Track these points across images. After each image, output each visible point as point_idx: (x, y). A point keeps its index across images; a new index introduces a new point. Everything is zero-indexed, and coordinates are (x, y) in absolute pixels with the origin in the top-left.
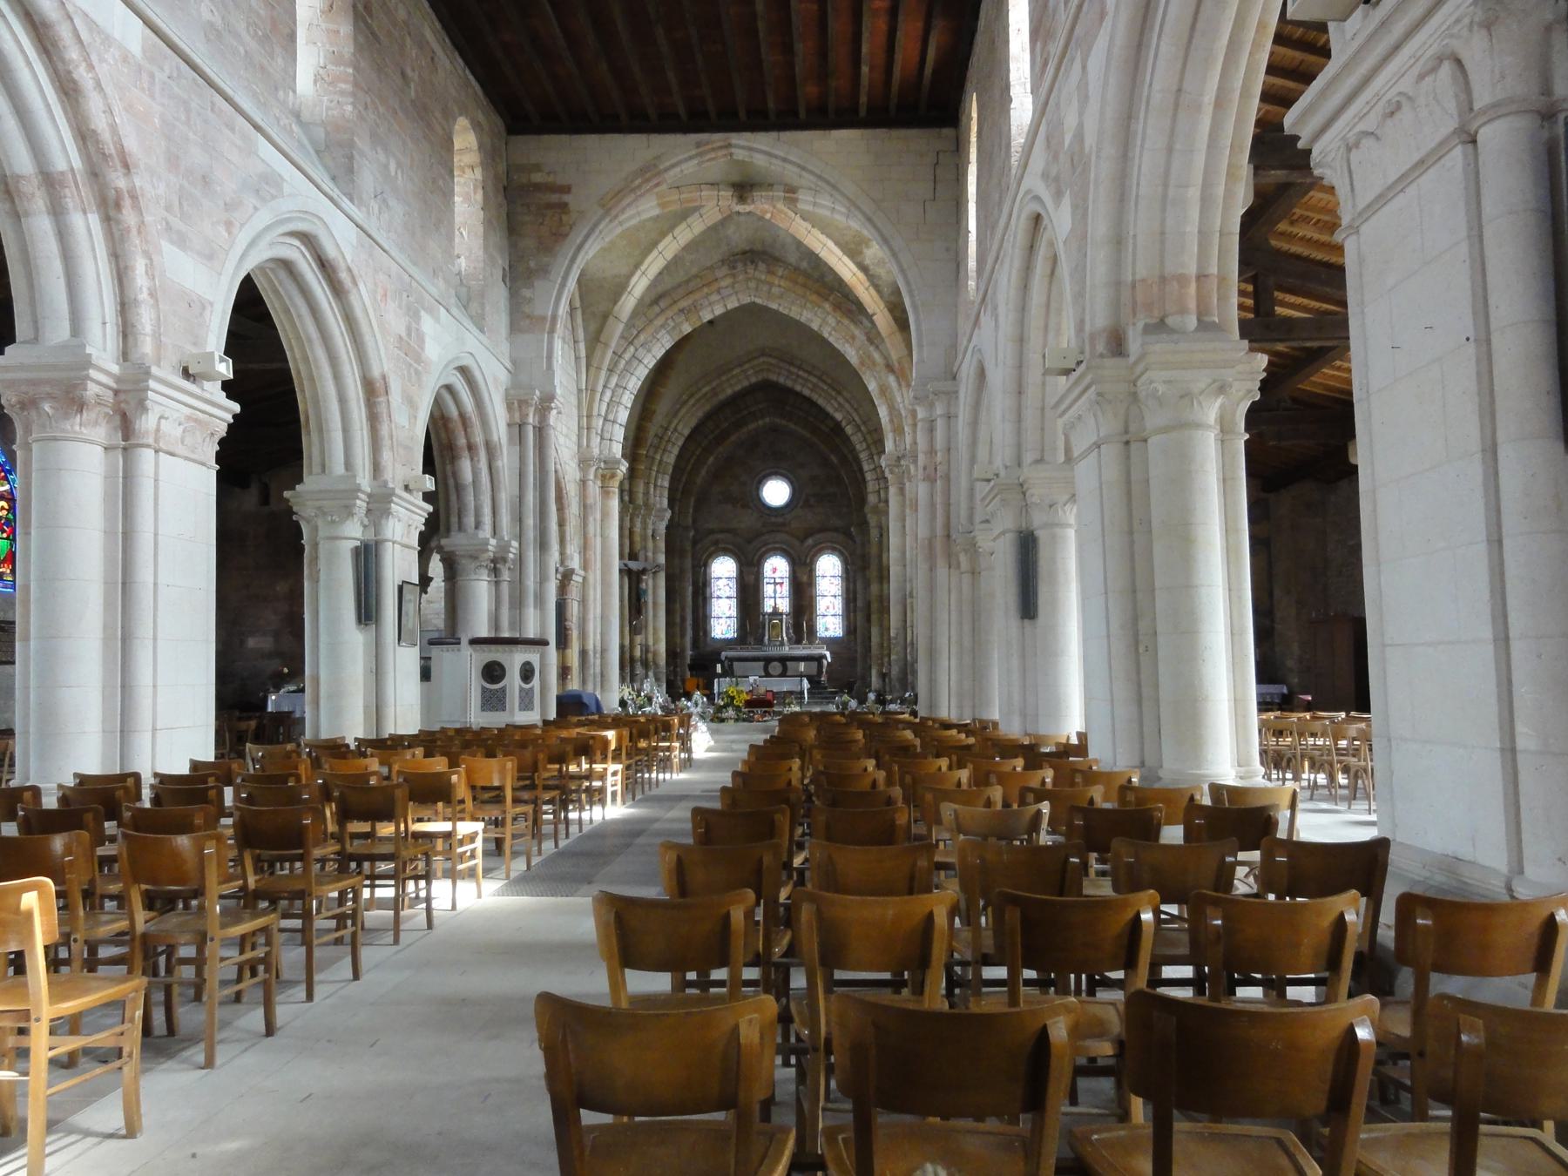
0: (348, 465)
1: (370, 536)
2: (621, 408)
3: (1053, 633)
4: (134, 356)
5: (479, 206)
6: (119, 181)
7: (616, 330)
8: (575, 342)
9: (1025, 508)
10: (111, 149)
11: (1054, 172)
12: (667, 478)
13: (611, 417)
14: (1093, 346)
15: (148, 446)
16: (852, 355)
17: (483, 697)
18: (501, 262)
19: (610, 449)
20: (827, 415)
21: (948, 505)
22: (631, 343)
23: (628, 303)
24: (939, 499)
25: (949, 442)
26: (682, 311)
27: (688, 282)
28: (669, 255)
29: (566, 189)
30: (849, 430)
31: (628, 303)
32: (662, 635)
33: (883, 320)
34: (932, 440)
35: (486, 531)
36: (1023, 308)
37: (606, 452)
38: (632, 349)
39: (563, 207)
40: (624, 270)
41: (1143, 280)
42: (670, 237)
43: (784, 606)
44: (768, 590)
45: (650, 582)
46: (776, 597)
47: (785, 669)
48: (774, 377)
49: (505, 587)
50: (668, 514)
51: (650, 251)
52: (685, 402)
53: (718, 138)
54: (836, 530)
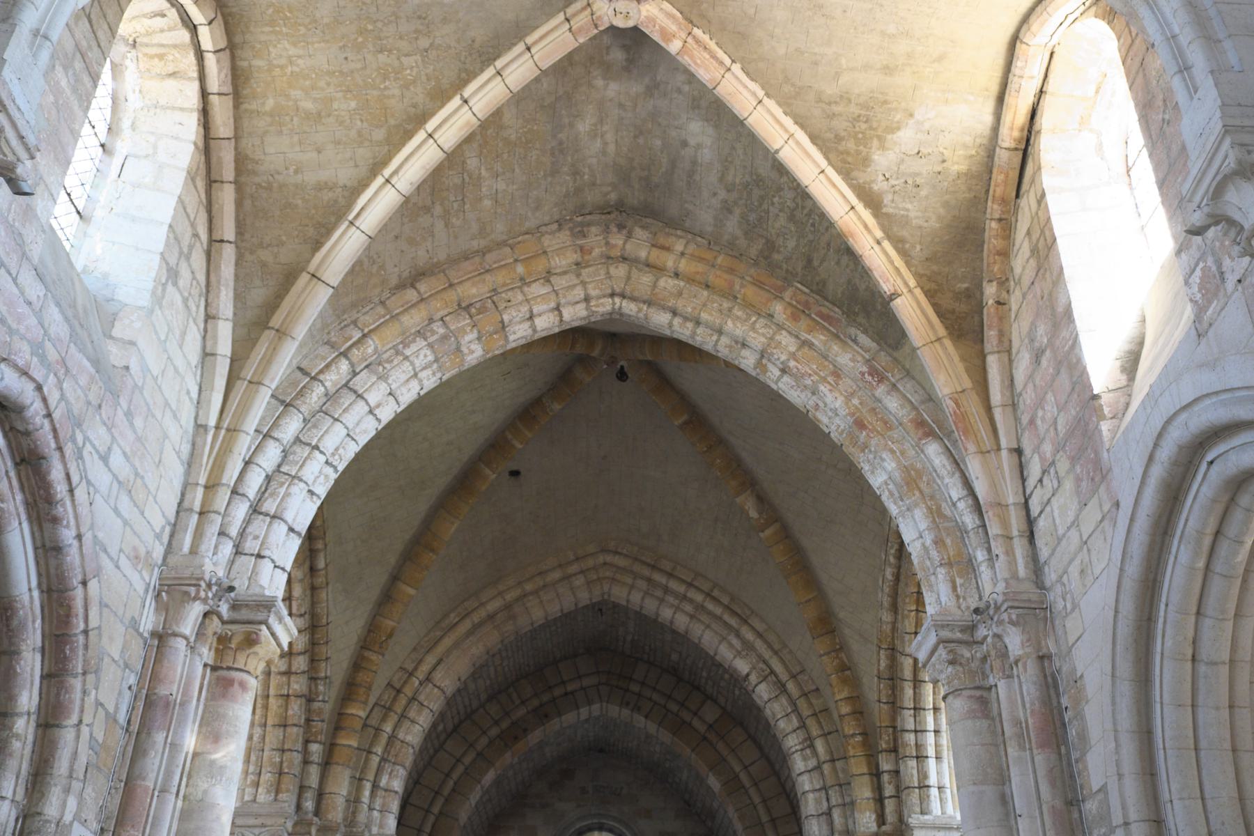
2: (298, 490)
7: (312, 304)
8: (209, 317)
12: (402, 772)
16: (832, 409)
23: (345, 247)
31: (345, 247)
38: (344, 366)
40: (345, 175)
42: (456, 101)
48: (619, 594)
51: (409, 135)
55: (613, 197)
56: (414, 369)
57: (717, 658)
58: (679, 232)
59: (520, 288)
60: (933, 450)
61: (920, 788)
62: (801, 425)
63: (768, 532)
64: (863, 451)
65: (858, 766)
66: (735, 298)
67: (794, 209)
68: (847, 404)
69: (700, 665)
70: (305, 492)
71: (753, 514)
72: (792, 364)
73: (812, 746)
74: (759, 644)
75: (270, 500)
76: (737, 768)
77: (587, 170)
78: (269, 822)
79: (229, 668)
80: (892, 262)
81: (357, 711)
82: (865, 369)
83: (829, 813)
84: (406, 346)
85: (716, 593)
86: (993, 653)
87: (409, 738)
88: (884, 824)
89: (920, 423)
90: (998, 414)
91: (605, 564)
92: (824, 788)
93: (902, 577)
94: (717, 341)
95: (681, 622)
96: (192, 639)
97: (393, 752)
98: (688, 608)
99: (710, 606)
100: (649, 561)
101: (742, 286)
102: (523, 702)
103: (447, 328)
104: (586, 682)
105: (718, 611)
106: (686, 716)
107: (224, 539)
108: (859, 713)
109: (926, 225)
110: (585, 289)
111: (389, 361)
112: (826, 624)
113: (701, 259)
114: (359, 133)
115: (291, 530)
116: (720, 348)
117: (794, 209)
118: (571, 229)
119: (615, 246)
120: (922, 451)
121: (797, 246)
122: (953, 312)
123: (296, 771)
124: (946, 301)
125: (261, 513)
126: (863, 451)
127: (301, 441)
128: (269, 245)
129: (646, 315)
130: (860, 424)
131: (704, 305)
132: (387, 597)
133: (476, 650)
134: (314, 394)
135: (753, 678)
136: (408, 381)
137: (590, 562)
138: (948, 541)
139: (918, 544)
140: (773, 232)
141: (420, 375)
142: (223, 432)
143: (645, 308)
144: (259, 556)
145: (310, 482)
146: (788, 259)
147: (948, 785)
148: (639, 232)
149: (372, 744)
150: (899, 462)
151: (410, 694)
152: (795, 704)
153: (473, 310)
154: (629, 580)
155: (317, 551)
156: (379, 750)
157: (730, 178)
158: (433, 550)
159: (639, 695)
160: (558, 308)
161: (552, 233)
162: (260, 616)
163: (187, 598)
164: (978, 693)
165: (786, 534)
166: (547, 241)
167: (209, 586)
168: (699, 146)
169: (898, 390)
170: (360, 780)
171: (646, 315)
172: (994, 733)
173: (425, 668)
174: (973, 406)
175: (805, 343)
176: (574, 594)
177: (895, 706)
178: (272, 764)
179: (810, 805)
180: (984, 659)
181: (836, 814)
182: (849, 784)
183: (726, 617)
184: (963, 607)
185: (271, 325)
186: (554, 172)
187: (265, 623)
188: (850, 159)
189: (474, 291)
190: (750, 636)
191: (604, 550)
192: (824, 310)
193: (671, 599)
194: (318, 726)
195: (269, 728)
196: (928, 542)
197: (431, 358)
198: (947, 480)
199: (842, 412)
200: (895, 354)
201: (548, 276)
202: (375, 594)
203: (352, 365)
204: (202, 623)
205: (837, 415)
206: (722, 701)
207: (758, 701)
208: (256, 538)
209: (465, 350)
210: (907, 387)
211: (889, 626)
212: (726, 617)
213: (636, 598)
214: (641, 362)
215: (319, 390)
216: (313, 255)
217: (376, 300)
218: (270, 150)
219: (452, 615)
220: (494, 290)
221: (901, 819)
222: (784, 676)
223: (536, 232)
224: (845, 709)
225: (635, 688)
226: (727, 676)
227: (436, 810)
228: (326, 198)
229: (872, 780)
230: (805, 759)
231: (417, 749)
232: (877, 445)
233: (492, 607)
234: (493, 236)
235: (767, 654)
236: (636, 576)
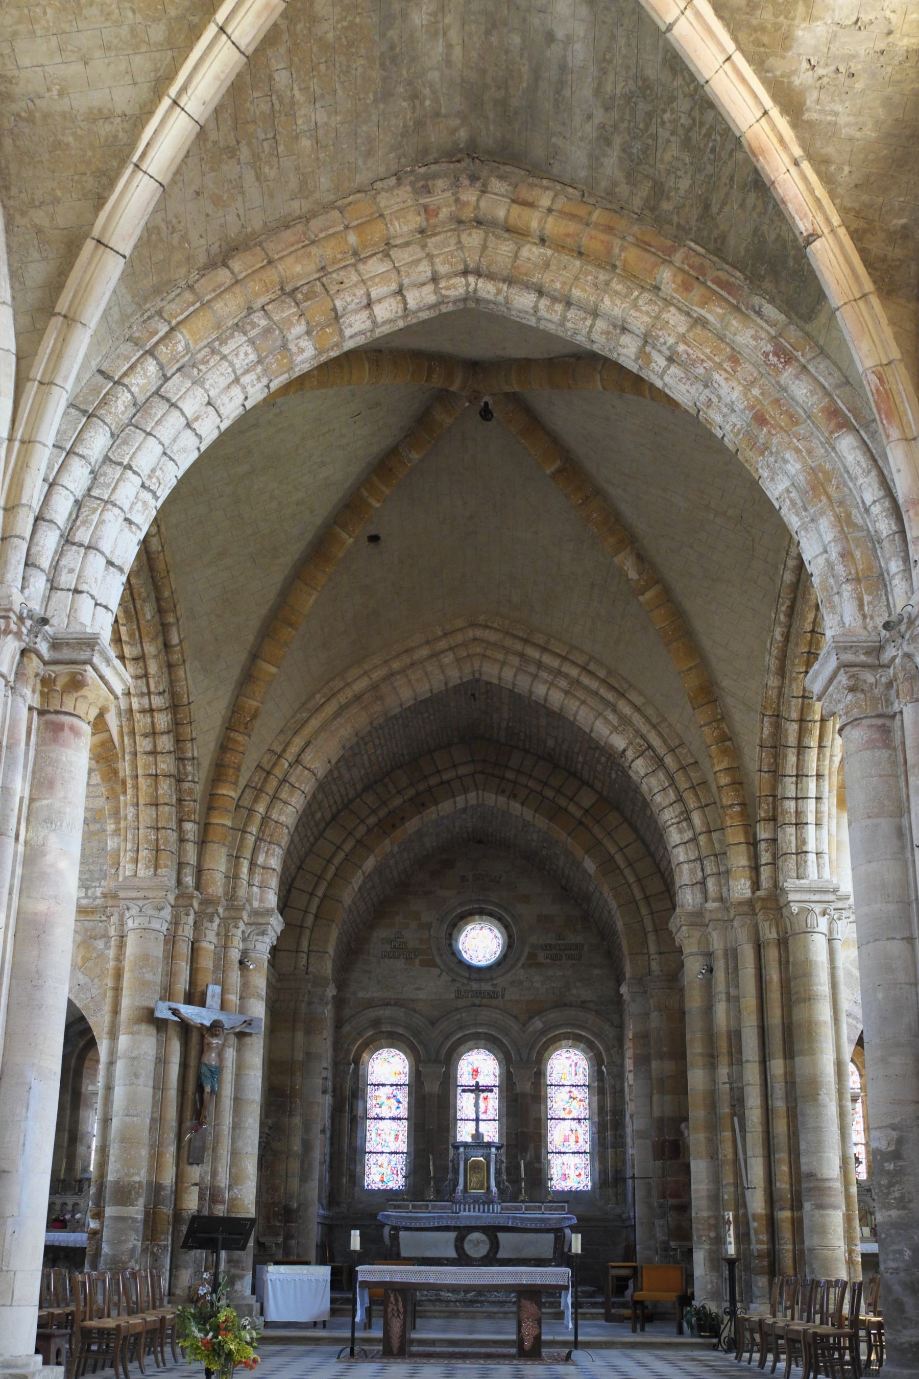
2: (113, 518)
7: (103, 280)
12: (278, 851)
23: (133, 203)
31: (133, 203)
32: (251, 1166)
38: (151, 366)
40: (123, 98)
43: (491, 1132)
44: (465, 1104)
45: (230, 1054)
46: (478, 1118)
47: (495, 1245)
48: (490, 672)
51: (195, 33)
54: (583, 1005)
55: (463, 134)
56: (234, 371)
57: (593, 735)
58: (545, 182)
59: (354, 265)
60: (846, 444)
61: (797, 854)
62: (691, 427)
63: (649, 594)
64: (762, 453)
65: (735, 835)
66: (614, 266)
67: (690, 129)
68: (745, 395)
69: (576, 750)
70: (121, 519)
71: (633, 575)
72: (681, 348)
73: (688, 819)
74: (637, 719)
75: (82, 529)
76: (613, 850)
77: (427, 91)
78: (150, 894)
79: (57, 712)
80: (812, 191)
81: (229, 792)
82: (769, 348)
83: (703, 883)
84: (223, 342)
85: (592, 667)
86: (901, 676)
87: (283, 819)
88: (758, 889)
89: (833, 413)
91: (475, 639)
92: (700, 859)
93: (792, 638)
94: (592, 326)
95: (556, 698)
96: (12, 678)
97: (267, 832)
98: (563, 683)
99: (586, 680)
100: (521, 634)
101: (622, 249)
102: (399, 792)
103: (270, 318)
104: (462, 770)
105: (594, 685)
106: (563, 802)
107: (32, 571)
108: (739, 783)
109: (858, 135)
110: (432, 264)
111: (205, 362)
112: (708, 694)
113: (572, 216)
114: (132, 30)
115: (110, 563)
116: (595, 336)
117: (690, 129)
118: (412, 184)
119: (466, 204)
120: (834, 449)
121: (692, 186)
122: (884, 259)
123: (174, 848)
124: (877, 246)
125: (73, 544)
126: (762, 453)
127: (111, 460)
128: (42, 203)
129: (506, 298)
130: (760, 420)
131: (577, 278)
132: (248, 678)
133: (344, 731)
134: (120, 402)
135: (630, 754)
136: (229, 387)
137: (459, 638)
138: (857, 554)
139: (821, 560)
140: (662, 167)
141: (242, 380)
142: (17, 444)
143: (505, 288)
144: (77, 591)
145: (126, 508)
146: (679, 209)
147: (826, 851)
148: (497, 185)
149: (246, 825)
150: (804, 463)
151: (281, 777)
152: (672, 779)
153: (300, 296)
154: (500, 656)
155: (169, 624)
156: (254, 829)
157: (609, 88)
158: (291, 625)
159: (515, 783)
160: (400, 292)
161: (390, 189)
162: (83, 656)
164: (880, 722)
165: (668, 597)
166: (383, 200)
167: (21, 619)
168: (569, 39)
169: (808, 371)
170: (238, 857)
171: (506, 298)
172: (894, 763)
173: (294, 749)
175: (700, 322)
176: (443, 672)
177: (776, 774)
178: (148, 841)
179: (685, 875)
180: (889, 685)
181: (711, 883)
182: (725, 854)
183: (603, 692)
184: (869, 627)
185: (57, 310)
186: (386, 96)
187: (89, 662)
188: (765, 39)
189: (298, 268)
190: (627, 710)
191: (473, 625)
193: (544, 675)
194: (189, 805)
195: (141, 808)
196: (834, 555)
197: (253, 357)
198: (861, 481)
199: (739, 406)
200: (808, 328)
201: (387, 249)
202: (235, 673)
203: (161, 367)
204: (20, 662)
205: (733, 411)
206: (598, 785)
207: (634, 777)
208: (71, 571)
209: (294, 349)
210: (819, 368)
211: (775, 691)
212: (603, 692)
213: (508, 674)
214: (507, 395)
215: (124, 397)
216: (97, 216)
217: (183, 284)
218: (25, 61)
219: (318, 696)
220: (323, 268)
221: (776, 885)
222: (661, 750)
223: (369, 189)
224: (724, 780)
225: (510, 775)
226: (603, 759)
227: (320, 892)
228: (102, 133)
229: (748, 850)
230: (681, 831)
231: (292, 829)
232: (779, 443)
233: (361, 685)
234: (317, 195)
235: (644, 728)
236: (507, 651)
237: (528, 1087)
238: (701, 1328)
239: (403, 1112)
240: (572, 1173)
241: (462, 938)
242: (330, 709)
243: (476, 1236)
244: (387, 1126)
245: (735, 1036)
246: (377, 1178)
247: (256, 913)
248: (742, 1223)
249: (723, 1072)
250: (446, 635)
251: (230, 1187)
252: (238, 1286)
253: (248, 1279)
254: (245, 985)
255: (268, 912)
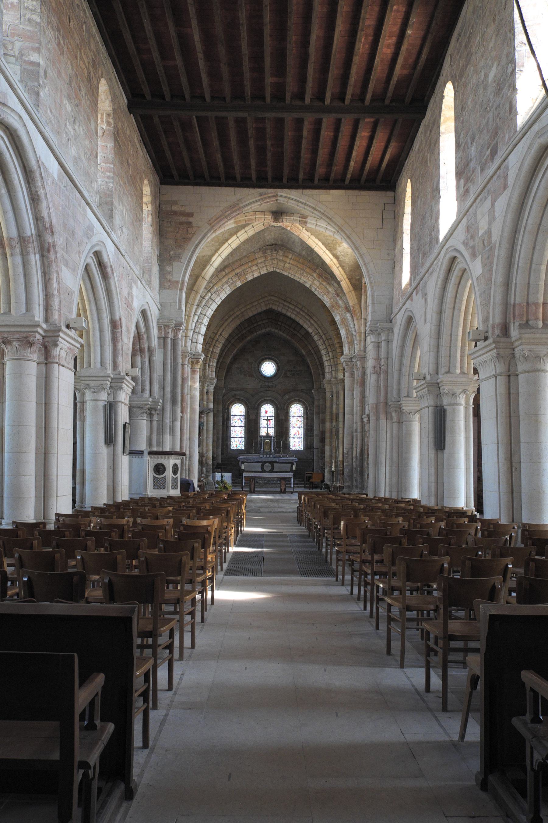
0: (102, 363)
1: (111, 399)
2: (203, 326)
3: (453, 456)
4: (51, 320)
5: (149, 225)
6: (49, 239)
9: (439, 395)
10: (48, 225)
11: (471, 243)
13: (197, 330)
14: (493, 331)
15: (56, 363)
16: (327, 301)
17: (154, 482)
18: (157, 252)
19: (196, 347)
20: (302, 327)
21: (386, 387)
22: (209, 291)
24: (382, 384)
25: (388, 353)
26: (237, 274)
27: (241, 259)
28: (234, 246)
29: (191, 215)
30: (316, 338)
32: (211, 448)
33: (345, 284)
34: (378, 353)
35: (147, 394)
36: (442, 298)
37: (194, 349)
39: (190, 223)
40: (209, 253)
41: (520, 304)
42: (235, 237)
43: (272, 432)
44: (263, 423)
46: (267, 428)
47: (273, 467)
48: (275, 307)
49: (155, 424)
50: (215, 381)
51: (224, 243)
52: (226, 320)
53: (271, 191)
54: (302, 391)
73: (328, 354)
74: (315, 325)
76: (311, 348)
84: (223, 286)
85: (303, 309)
87: (217, 351)
90: (362, 309)
92: (331, 365)
105: (304, 314)
106: (296, 332)
133: (234, 326)
137: (266, 299)
156: (209, 355)
161: (258, 253)
163: (186, 357)
173: (220, 332)
174: (357, 308)
179: (327, 369)
181: (333, 373)
183: (307, 317)
190: (313, 322)
191: (270, 295)
192: (326, 276)
212: (307, 317)
222: (322, 334)
224: (337, 345)
235: (317, 328)
237: (283, 417)
238: (325, 488)
239: (243, 424)
240: (297, 444)
241: (262, 367)
242: (229, 320)
243: (267, 464)
244: (238, 429)
245: (337, 414)
246: (235, 446)
247: (211, 379)
248: (336, 462)
249: (334, 424)
250: (262, 298)
251: (206, 453)
252: (209, 478)
253: (211, 476)
254: (208, 399)
255: (214, 379)
